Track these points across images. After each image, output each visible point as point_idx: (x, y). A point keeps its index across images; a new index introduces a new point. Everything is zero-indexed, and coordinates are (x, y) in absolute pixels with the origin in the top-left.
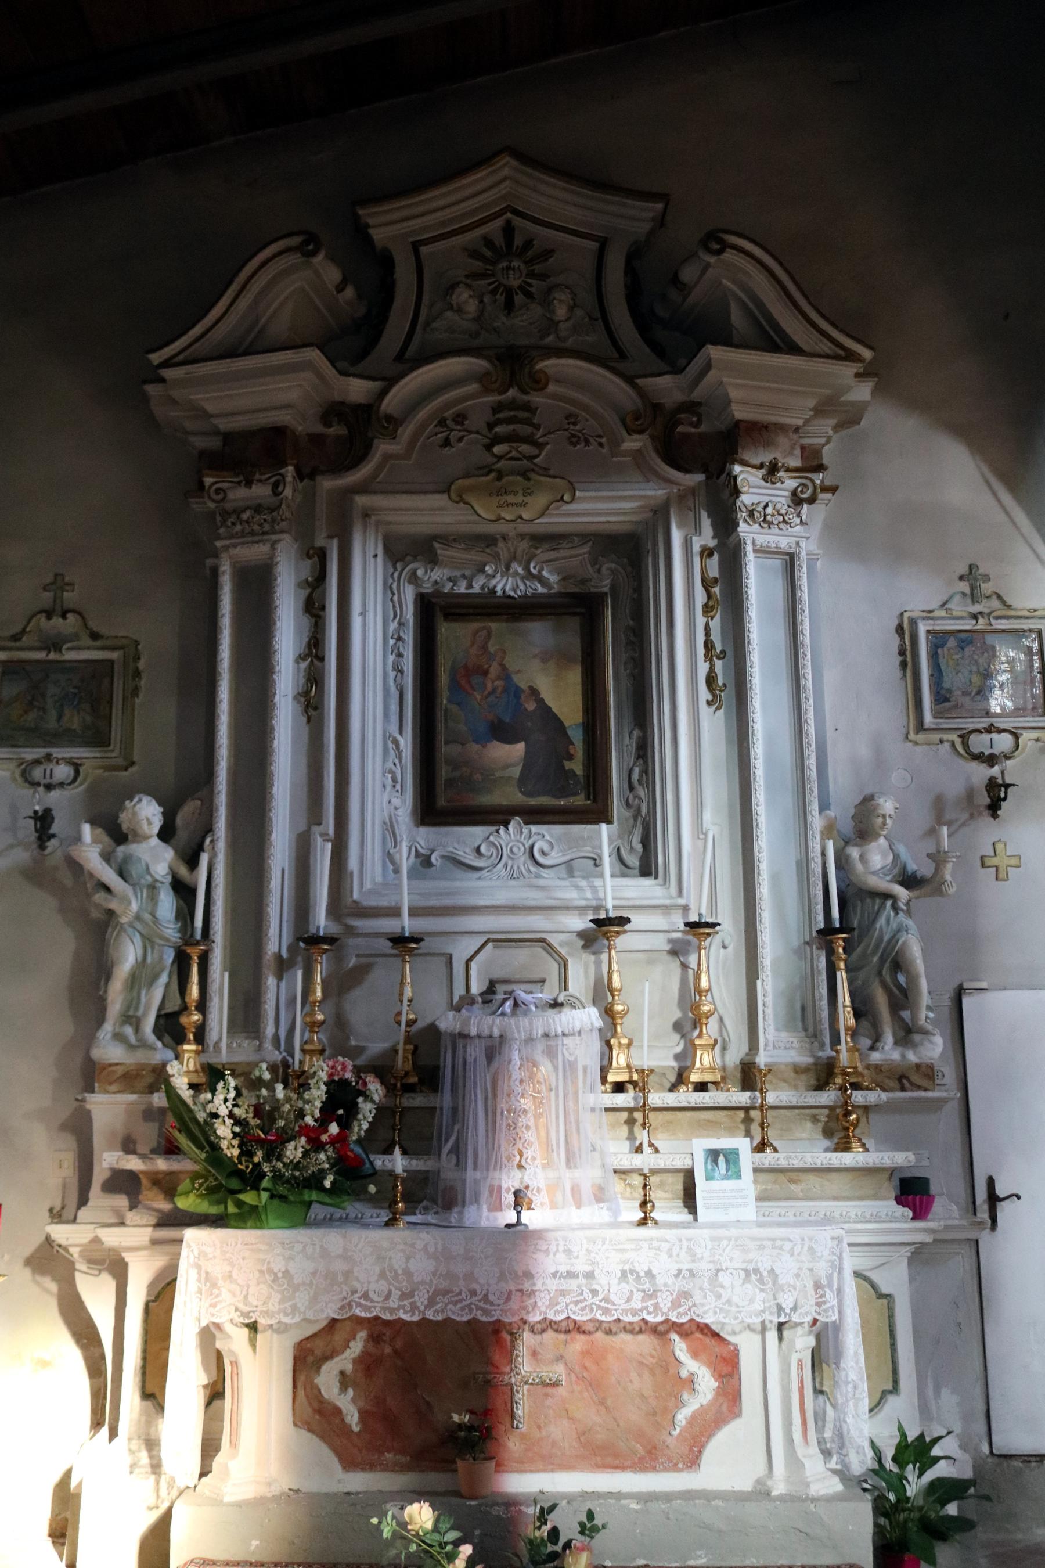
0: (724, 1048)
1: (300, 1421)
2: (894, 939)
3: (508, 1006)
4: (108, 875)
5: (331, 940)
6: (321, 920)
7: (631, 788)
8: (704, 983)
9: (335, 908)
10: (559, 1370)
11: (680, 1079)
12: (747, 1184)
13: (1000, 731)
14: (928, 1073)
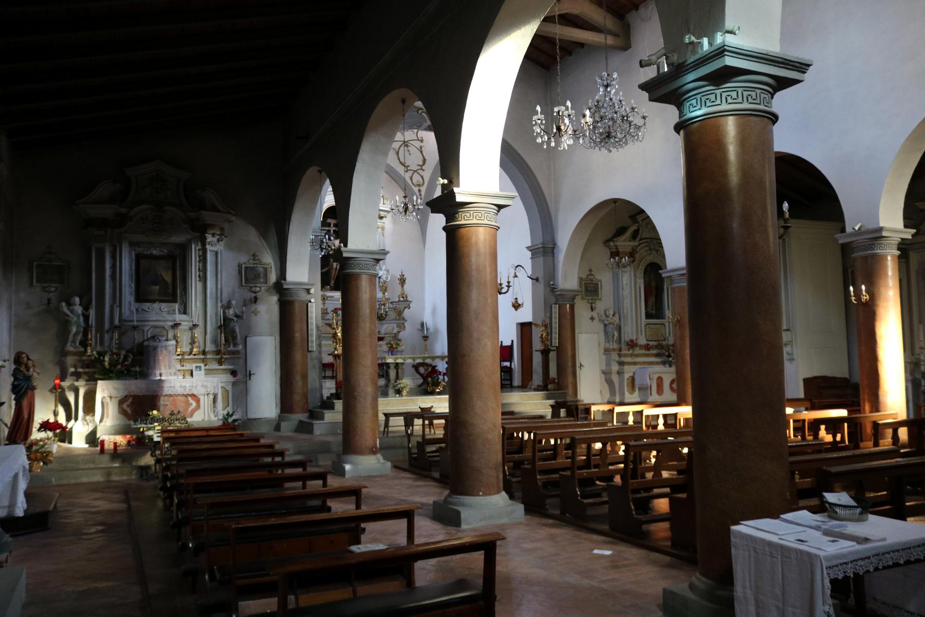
0: (199, 348)
1: (120, 413)
2: (233, 328)
3: (157, 341)
4: (68, 312)
5: (119, 327)
6: (117, 322)
7: (182, 296)
8: (196, 335)
9: (120, 321)
10: (168, 403)
11: (191, 353)
12: (203, 372)
13: (257, 287)
14: (238, 352)
